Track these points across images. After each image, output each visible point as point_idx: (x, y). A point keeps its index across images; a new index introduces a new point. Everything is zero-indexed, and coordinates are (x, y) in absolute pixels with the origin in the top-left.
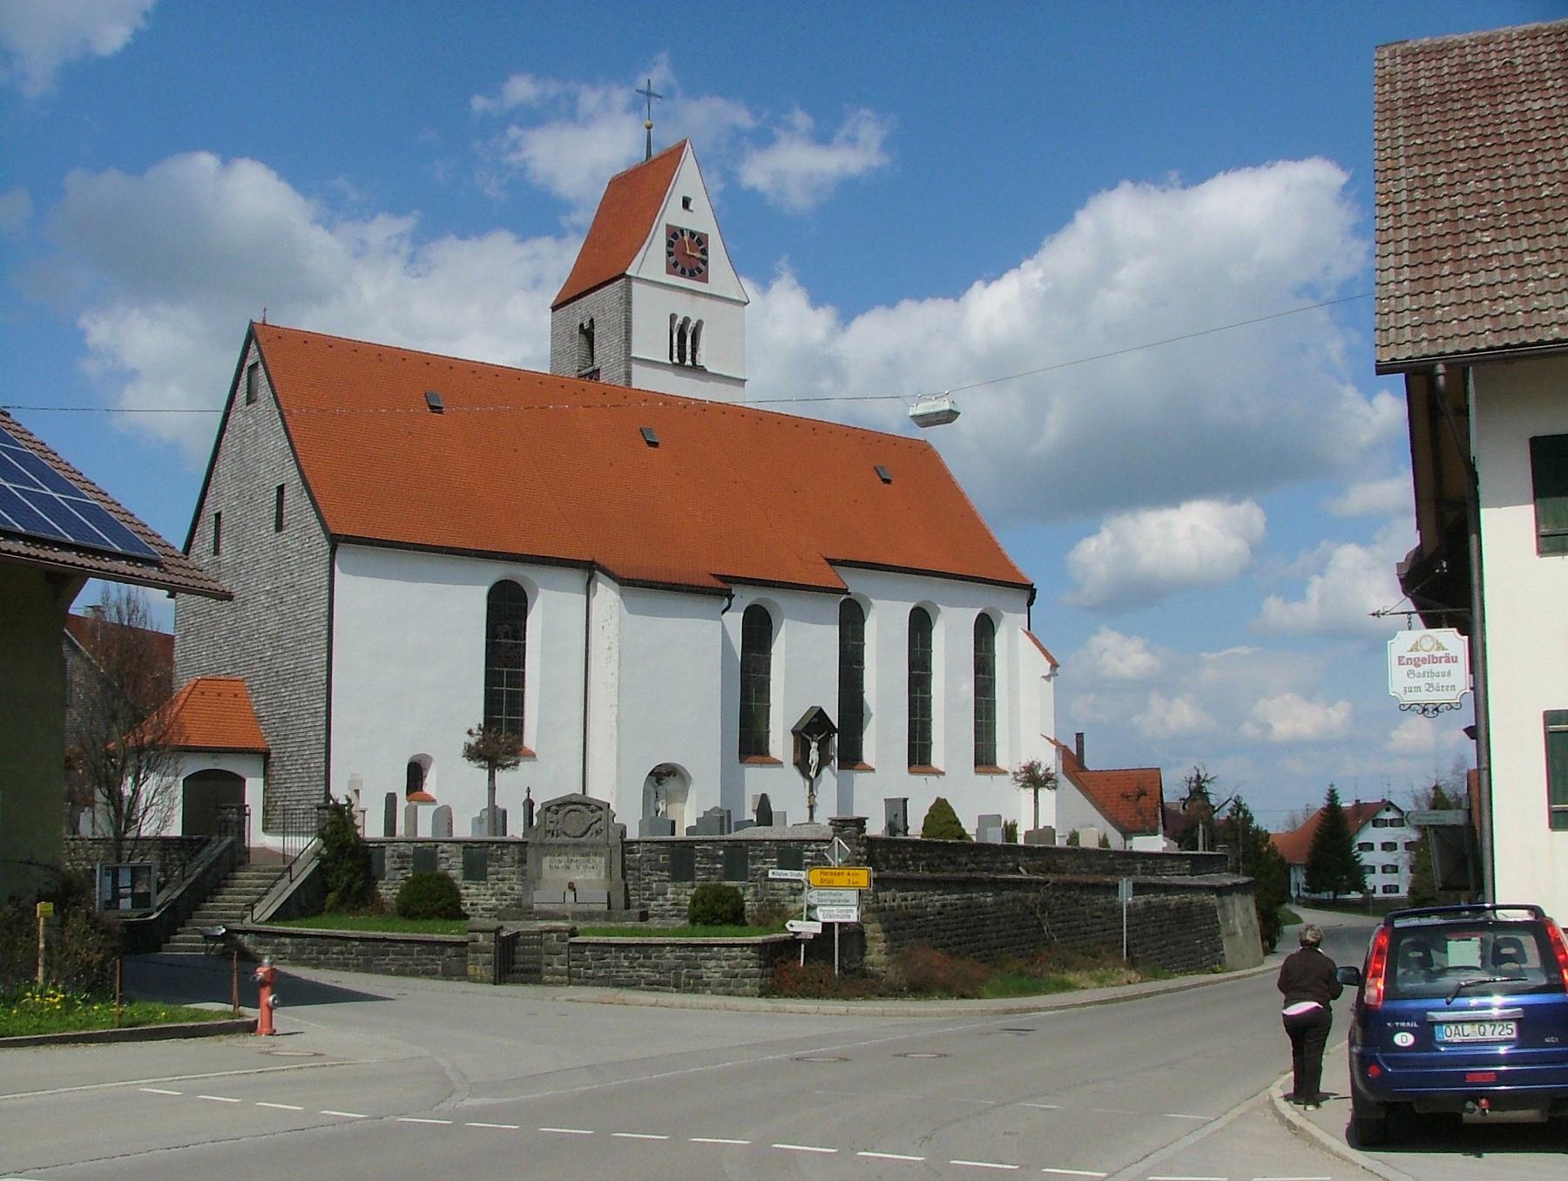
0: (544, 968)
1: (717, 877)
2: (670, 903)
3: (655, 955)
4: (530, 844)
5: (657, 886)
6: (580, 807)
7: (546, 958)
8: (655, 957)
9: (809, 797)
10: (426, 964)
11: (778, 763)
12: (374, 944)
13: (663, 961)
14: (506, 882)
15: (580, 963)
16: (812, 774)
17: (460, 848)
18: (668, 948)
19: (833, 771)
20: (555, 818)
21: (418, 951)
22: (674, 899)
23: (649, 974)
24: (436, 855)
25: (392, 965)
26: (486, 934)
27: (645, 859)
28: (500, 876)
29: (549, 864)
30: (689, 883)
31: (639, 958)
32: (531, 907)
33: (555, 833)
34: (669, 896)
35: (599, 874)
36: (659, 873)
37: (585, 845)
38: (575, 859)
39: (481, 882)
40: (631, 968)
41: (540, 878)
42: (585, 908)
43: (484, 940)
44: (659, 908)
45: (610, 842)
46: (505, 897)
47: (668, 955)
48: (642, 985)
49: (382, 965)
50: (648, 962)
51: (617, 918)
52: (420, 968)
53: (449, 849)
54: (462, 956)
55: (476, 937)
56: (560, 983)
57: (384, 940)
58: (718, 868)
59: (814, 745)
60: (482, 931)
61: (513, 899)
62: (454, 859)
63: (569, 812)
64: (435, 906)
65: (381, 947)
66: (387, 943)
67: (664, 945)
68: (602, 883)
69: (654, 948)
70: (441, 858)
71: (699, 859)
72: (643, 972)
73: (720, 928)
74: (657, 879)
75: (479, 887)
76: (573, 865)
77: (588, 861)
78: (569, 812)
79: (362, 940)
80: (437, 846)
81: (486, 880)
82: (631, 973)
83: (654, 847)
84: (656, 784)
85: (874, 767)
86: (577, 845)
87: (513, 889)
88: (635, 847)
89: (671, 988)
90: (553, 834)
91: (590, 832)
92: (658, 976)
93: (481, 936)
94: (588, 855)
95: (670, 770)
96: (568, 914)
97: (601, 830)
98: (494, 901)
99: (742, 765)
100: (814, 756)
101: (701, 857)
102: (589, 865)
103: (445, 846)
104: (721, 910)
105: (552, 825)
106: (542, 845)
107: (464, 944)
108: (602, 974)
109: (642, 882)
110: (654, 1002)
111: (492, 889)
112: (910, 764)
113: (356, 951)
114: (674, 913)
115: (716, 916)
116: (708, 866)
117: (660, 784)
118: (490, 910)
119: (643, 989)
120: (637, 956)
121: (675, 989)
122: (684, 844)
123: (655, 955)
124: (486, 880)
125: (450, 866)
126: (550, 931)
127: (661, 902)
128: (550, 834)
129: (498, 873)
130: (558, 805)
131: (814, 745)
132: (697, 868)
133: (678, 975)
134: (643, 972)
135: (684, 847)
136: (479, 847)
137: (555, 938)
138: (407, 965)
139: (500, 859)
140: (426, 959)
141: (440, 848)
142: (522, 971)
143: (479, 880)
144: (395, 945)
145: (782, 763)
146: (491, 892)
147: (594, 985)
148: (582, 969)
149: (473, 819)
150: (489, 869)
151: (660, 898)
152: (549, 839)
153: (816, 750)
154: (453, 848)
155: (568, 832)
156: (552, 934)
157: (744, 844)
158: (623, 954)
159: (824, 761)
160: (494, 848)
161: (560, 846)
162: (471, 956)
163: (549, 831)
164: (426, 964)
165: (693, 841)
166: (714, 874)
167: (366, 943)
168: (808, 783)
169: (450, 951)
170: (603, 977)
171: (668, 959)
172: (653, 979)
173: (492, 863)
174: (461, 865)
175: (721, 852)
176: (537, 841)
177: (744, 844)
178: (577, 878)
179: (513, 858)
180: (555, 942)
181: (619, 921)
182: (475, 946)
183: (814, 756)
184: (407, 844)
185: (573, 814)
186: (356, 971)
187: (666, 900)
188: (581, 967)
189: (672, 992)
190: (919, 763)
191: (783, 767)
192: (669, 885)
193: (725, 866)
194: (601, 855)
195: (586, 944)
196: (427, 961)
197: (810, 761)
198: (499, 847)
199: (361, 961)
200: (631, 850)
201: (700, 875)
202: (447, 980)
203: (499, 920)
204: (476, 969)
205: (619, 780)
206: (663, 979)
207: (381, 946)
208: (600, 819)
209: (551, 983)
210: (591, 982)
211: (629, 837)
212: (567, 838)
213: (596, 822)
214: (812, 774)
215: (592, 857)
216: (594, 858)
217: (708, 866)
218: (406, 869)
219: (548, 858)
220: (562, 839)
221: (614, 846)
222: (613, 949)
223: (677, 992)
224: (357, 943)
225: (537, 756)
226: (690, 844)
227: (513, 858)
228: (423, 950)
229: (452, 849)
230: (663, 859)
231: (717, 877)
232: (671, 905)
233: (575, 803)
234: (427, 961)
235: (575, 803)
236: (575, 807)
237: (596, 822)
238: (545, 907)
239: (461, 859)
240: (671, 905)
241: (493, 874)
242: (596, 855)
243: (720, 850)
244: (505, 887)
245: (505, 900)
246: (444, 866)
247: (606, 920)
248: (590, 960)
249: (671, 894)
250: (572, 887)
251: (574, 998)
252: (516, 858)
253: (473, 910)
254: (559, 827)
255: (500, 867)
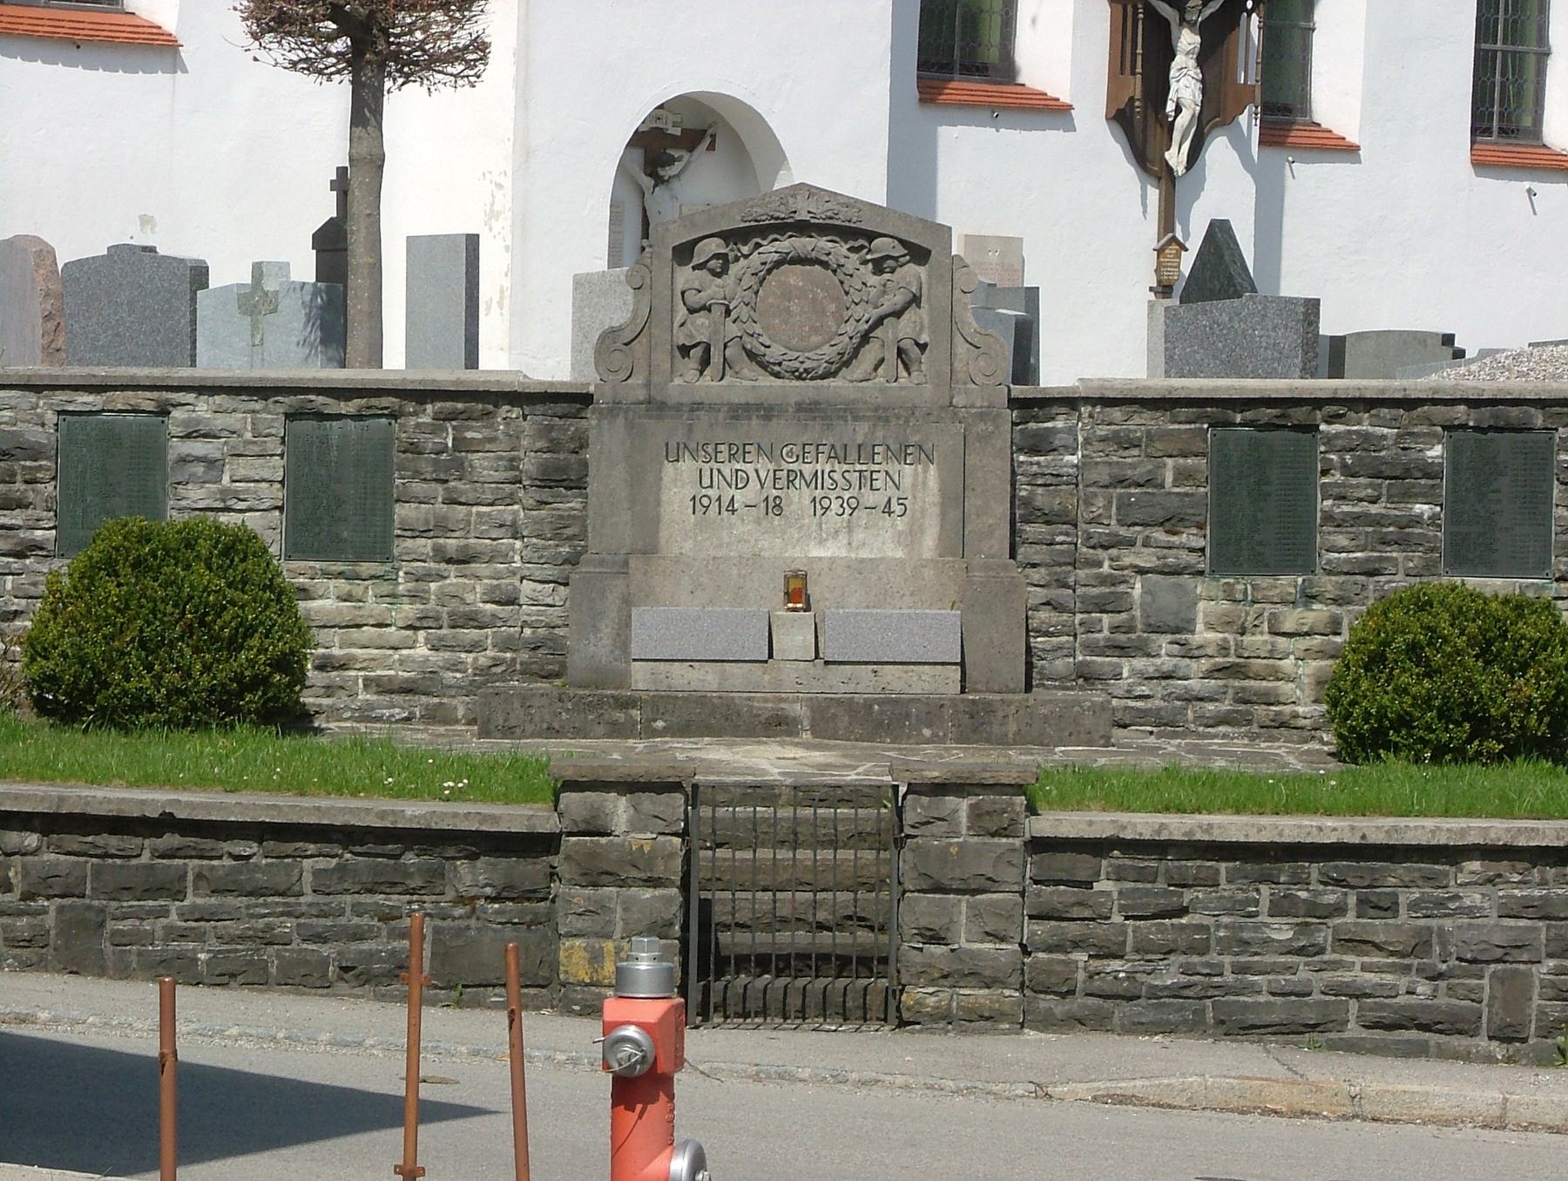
0: (914, 954)
1: (1416, 558)
2: (1205, 664)
3: (1416, 894)
4: (601, 402)
5: (1146, 591)
6: (823, 243)
7: (921, 909)
8: (1413, 906)
9: (1160, 251)
10: (358, 936)
11: (1051, 112)
12: (113, 842)
13: (1448, 924)
14: (474, 567)
15: (1073, 929)
16: (1176, 157)
17: (272, 416)
18: (1476, 865)
19: (1240, 145)
20: (714, 289)
21: (317, 873)
22: (1223, 649)
23: (1389, 978)
24: (162, 450)
25: (200, 937)
26: (648, 801)
27: (1103, 475)
28: (452, 544)
29: (689, 492)
30: (1288, 583)
31: (1339, 909)
32: (623, 679)
33: (716, 359)
34: (1202, 635)
35: (912, 536)
36: (1159, 535)
37: (849, 411)
38: (808, 470)
39: (366, 568)
40: (1300, 951)
41: (649, 550)
42: (864, 683)
43: (635, 826)
44: (1158, 688)
45: (959, 400)
46: (472, 634)
47: (1473, 898)
48: (1353, 1031)
49: (150, 937)
50: (1378, 928)
51: (1012, 728)
52: (326, 950)
53: (221, 421)
54: (529, 895)
55: (596, 812)
56: (982, 1020)
57: (165, 823)
58: (1417, 521)
59: (1188, 40)
60: (630, 787)
61: (506, 644)
62: (243, 467)
63: (778, 264)
64: (223, 673)
65: (145, 858)
66: (172, 840)
67: (1452, 854)
68: (928, 573)
69: (1402, 869)
70: (184, 460)
71: (1337, 477)
72: (1357, 970)
73: (1495, 771)
74: (1146, 559)
75: (357, 588)
76: (799, 498)
77: (867, 480)
78: (778, 264)
79: (51, 824)
80: (163, 411)
81: (388, 558)
82: (1303, 974)
83: (1141, 423)
84: (648, 182)
85: (1352, 138)
86: (810, 410)
87: (512, 601)
88: (1059, 424)
89: (1482, 1043)
90: (705, 362)
91: (870, 354)
92: (1423, 988)
93: (620, 810)
94: (865, 452)
95: (691, 124)
96: (799, 710)
97: (923, 347)
98: (422, 651)
99: (931, 112)
100: (1185, 86)
101: (1348, 471)
102: (869, 498)
103: (203, 408)
104: (1505, 703)
105: (701, 319)
106: (656, 407)
107: (540, 844)
108: (1169, 976)
109: (1082, 573)
110: (1495, 1111)
111: (413, 596)
112: (1479, 128)
113: (26, 873)
114: (1226, 706)
115: (1482, 726)
116: (1374, 509)
117: (659, 181)
118: (408, 689)
119: (1352, 1047)
120: (1331, 897)
121: (1498, 1049)
122: (1268, 413)
123: (1416, 894)
124: (388, 558)
125: (224, 494)
126: (939, 789)
127: (1166, 663)
128: (693, 362)
129: (442, 527)
130: (727, 236)
131: (1188, 40)
132: (1329, 517)
133: (1513, 988)
134: (1357, 970)
135: (1270, 426)
136: (358, 417)
137: (963, 817)
138: (268, 939)
139: (452, 467)
140: (358, 910)
141: (177, 414)
142: (763, 963)
143: (360, 558)
144: (208, 844)
145: (1068, 108)
146: (408, 610)
147: (1135, 1028)
148: (1081, 957)
149: (1012, 245)
150: (402, 511)
151: (1163, 642)
152: (686, 382)
153: (1192, 63)
154: (237, 417)
155: (774, 353)
156: (951, 800)
157: (1538, 419)
158: (1265, 890)
159: (1215, 114)
160: (425, 419)
161: (739, 412)
162: (581, 896)
163: (685, 350)
164: (358, 936)
165: (1317, 403)
166: (1403, 542)
167: (74, 841)
168: (1154, 194)
169: (472, 875)
170: (1177, 992)
171: (1470, 912)
172: (1402, 1000)
173: (417, 487)
174: (276, 494)
175: (1436, 452)
176: (635, 389)
177: (1538, 419)
178: (817, 552)
179: (513, 464)
180: (964, 836)
181: (1020, 740)
182: (593, 854)
183: (1185, 86)
184: (32, 397)
185: (793, 276)
186: (27, 966)
187: (1189, 653)
188: (1077, 945)
189: (1490, 1059)
190: (1502, 131)
191: (1071, 128)
192: (1201, 587)
193: (1454, 516)
194: (924, 454)
195: (1098, 847)
196: (365, 921)
197: (1170, 107)
198: (451, 417)
199: (50, 920)
200: (1036, 434)
201: (1338, 548)
202: (459, 1004)
203: (484, 733)
204: (596, 958)
205: (525, 152)
206: (1443, 1001)
207: (146, 851)
208: (915, 300)
209: (945, 1019)
210: (1121, 1010)
211: (1055, 373)
212: (767, 381)
213: (898, 314)
214: (1176, 157)
215: (883, 466)
216: (893, 467)
217: (1374, 509)
218: (21, 504)
219: (687, 466)
220: (750, 384)
221: (982, 417)
222: (1223, 866)
223: (1509, 1060)
224: (32, 840)
225: (183, 52)
226: (1299, 415)
227: (513, 464)
228: (342, 869)
229: (232, 421)
230: (1182, 476)
231: (1416, 558)
232: (1209, 675)
233: (803, 228)
234: (365, 921)
235: (803, 228)
236: (787, 244)
237: (898, 314)
238: (683, 678)
239: (275, 467)
240: (1209, 675)
241: (424, 533)
242: (901, 454)
243: (1433, 439)
244: (473, 590)
245: (473, 647)
246: (197, 495)
247: (961, 739)
248: (1117, 919)
249: (1210, 627)
250: (797, 592)
251: (1137, 1086)
252: (529, 464)
253: (329, 690)
254: (733, 329)
255: (452, 501)
